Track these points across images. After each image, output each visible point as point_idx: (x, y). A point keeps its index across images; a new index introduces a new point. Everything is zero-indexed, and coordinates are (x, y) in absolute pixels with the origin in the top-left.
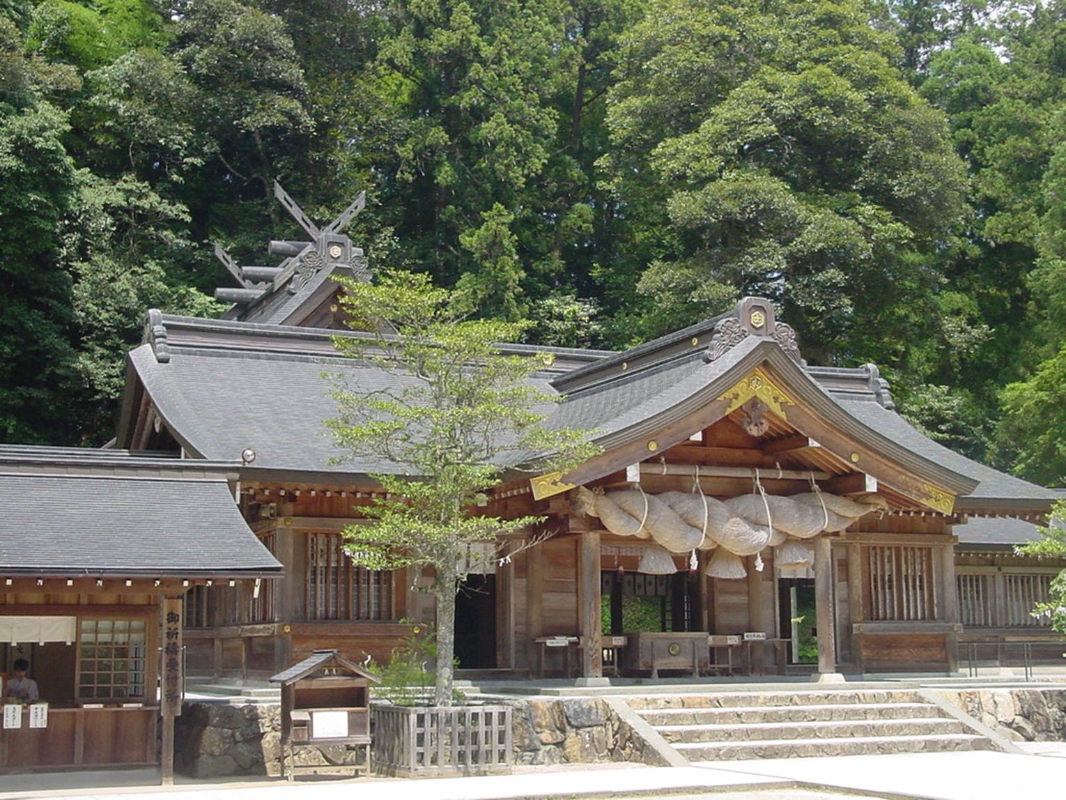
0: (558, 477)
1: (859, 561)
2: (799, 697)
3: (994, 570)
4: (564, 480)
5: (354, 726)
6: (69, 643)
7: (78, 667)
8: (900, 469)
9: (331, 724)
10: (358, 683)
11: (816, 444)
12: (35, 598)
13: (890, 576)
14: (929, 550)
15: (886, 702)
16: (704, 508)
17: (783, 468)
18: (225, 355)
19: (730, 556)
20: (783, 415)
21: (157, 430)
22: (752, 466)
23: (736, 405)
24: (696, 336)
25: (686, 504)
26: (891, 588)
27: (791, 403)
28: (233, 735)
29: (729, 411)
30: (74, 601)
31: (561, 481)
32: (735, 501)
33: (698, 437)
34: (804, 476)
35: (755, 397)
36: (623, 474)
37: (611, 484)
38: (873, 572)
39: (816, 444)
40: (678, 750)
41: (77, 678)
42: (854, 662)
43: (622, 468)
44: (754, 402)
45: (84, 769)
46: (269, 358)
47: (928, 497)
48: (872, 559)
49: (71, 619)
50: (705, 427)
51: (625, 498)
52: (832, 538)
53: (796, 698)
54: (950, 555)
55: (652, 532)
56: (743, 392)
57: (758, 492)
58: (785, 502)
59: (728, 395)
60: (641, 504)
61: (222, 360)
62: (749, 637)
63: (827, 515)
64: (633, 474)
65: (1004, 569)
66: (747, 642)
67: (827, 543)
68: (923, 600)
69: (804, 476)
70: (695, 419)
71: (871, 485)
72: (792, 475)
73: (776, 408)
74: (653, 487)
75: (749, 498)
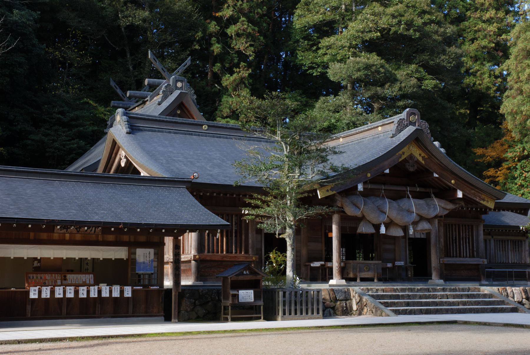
0: (329, 188)
1: (443, 231)
2: (432, 289)
3: (490, 237)
4: (332, 189)
5: (256, 296)
6: (125, 259)
7: (129, 270)
8: (472, 187)
9: (247, 295)
10: (258, 277)
11: (437, 176)
12: (111, 238)
13: (456, 238)
14: (472, 226)
15: (468, 292)
16: (387, 205)
17: (419, 186)
18: (155, 131)
19: (397, 225)
20: (423, 162)
21: (123, 164)
22: (406, 185)
23: (403, 157)
24: (381, 126)
25: (380, 202)
26: (456, 243)
27: (426, 157)
28: (195, 302)
29: (400, 160)
30: (128, 240)
31: (330, 190)
32: (399, 201)
33: (387, 171)
34: (428, 190)
35: (412, 154)
36: (356, 187)
37: (350, 192)
38: (448, 236)
39: (437, 176)
40: (390, 310)
41: (130, 275)
42: (450, 274)
43: (355, 185)
44: (411, 156)
45: (133, 316)
46: (175, 133)
47: (484, 200)
48: (448, 230)
49: (126, 248)
50: (390, 167)
51: (354, 198)
52: (439, 218)
53: (430, 289)
54: (481, 228)
55: (365, 214)
56: (406, 152)
57: (409, 197)
58: (421, 202)
59: (400, 152)
60: (360, 201)
61: (154, 133)
62: (398, 263)
63: (438, 207)
64: (360, 187)
65: (495, 237)
66: (396, 266)
67: (436, 221)
68: (469, 249)
69: (428, 190)
70: (386, 163)
71: (460, 194)
72: (423, 190)
73: (420, 159)
74: (365, 194)
75: (405, 200)
